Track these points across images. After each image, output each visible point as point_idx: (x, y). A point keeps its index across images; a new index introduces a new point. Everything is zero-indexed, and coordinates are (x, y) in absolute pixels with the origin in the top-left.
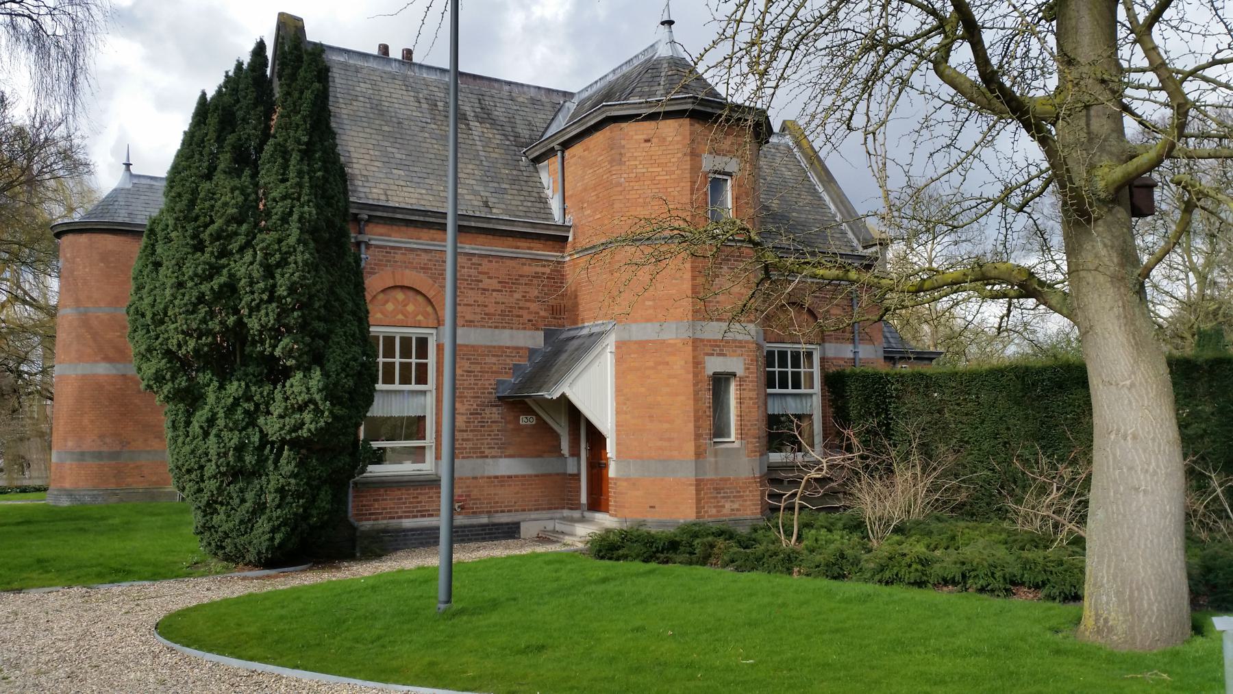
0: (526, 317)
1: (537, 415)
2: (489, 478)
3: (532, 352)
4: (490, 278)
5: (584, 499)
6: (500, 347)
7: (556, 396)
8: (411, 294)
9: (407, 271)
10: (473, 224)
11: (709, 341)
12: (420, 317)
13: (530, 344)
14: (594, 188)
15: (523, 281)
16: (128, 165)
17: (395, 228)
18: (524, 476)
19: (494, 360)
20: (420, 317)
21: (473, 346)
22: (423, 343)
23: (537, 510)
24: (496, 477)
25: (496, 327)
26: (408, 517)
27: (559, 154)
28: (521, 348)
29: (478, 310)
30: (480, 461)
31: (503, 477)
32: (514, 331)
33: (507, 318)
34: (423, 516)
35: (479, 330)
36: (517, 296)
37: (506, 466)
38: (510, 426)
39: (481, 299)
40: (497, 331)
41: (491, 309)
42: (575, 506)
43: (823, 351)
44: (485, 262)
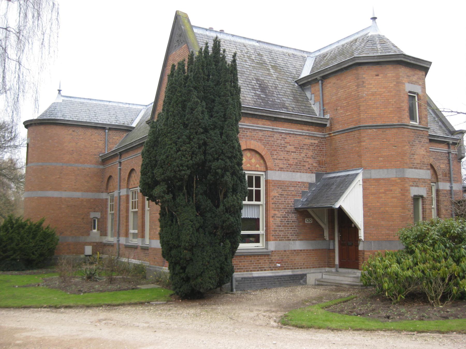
0: (307, 166)
1: (313, 218)
2: (292, 251)
3: (311, 185)
4: (290, 145)
5: (337, 262)
6: (295, 182)
7: (337, 206)
8: (253, 153)
9: (252, 141)
10: (283, 117)
11: (412, 179)
12: (258, 166)
13: (309, 181)
14: (346, 99)
15: (306, 147)
16: (59, 91)
17: (246, 118)
18: (307, 250)
19: (293, 189)
20: (258, 166)
21: (283, 181)
22: (258, 179)
23: (313, 268)
24: (295, 251)
25: (294, 171)
26: (254, 271)
27: (320, 82)
28: (305, 183)
29: (285, 162)
30: (287, 242)
31: (298, 250)
32: (302, 174)
33: (298, 167)
34: (262, 270)
35: (286, 173)
36: (303, 155)
37: (298, 245)
38: (301, 224)
39: (286, 156)
40: (294, 174)
41: (291, 162)
42: (333, 266)
43: (438, 186)
44: (288, 137)
